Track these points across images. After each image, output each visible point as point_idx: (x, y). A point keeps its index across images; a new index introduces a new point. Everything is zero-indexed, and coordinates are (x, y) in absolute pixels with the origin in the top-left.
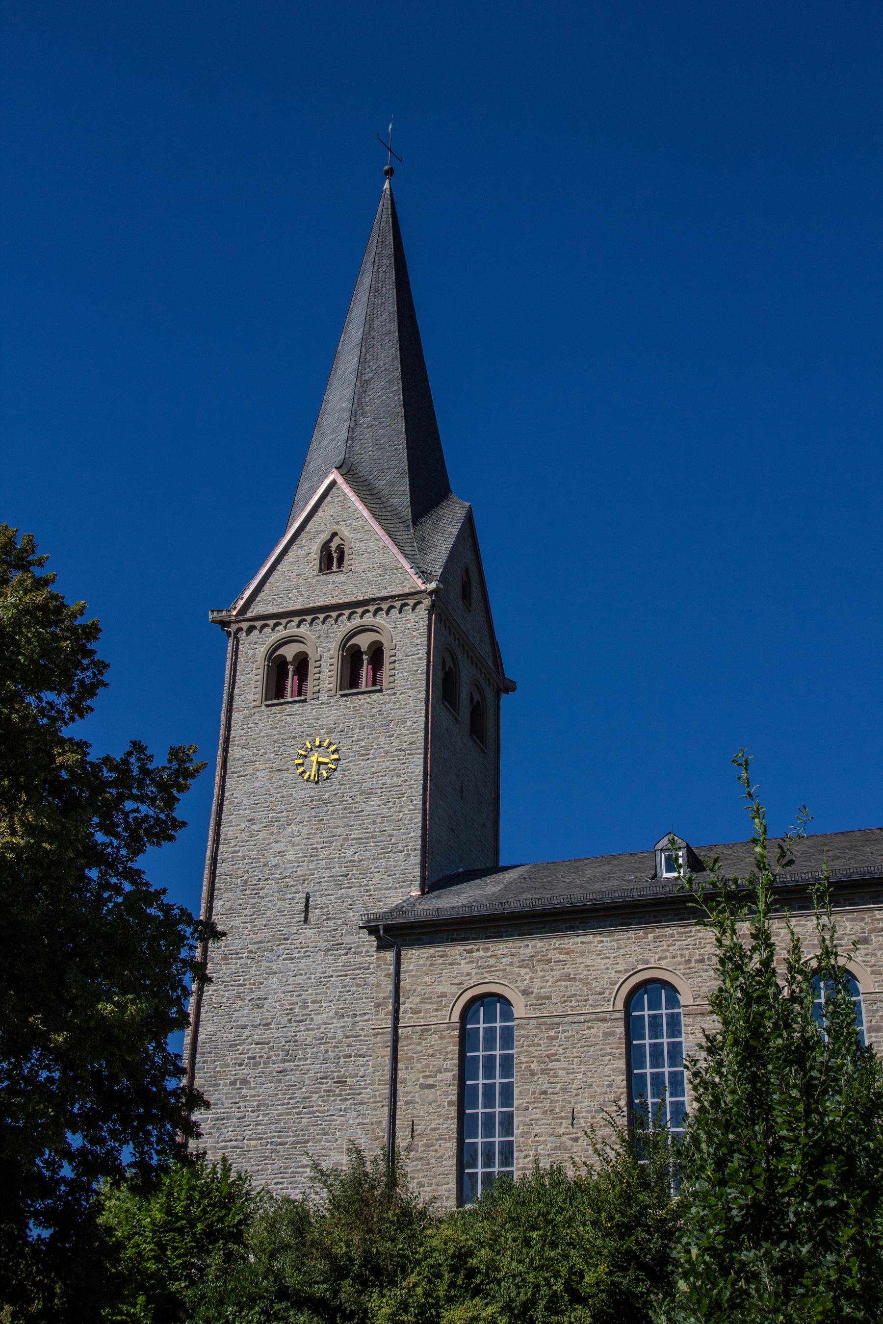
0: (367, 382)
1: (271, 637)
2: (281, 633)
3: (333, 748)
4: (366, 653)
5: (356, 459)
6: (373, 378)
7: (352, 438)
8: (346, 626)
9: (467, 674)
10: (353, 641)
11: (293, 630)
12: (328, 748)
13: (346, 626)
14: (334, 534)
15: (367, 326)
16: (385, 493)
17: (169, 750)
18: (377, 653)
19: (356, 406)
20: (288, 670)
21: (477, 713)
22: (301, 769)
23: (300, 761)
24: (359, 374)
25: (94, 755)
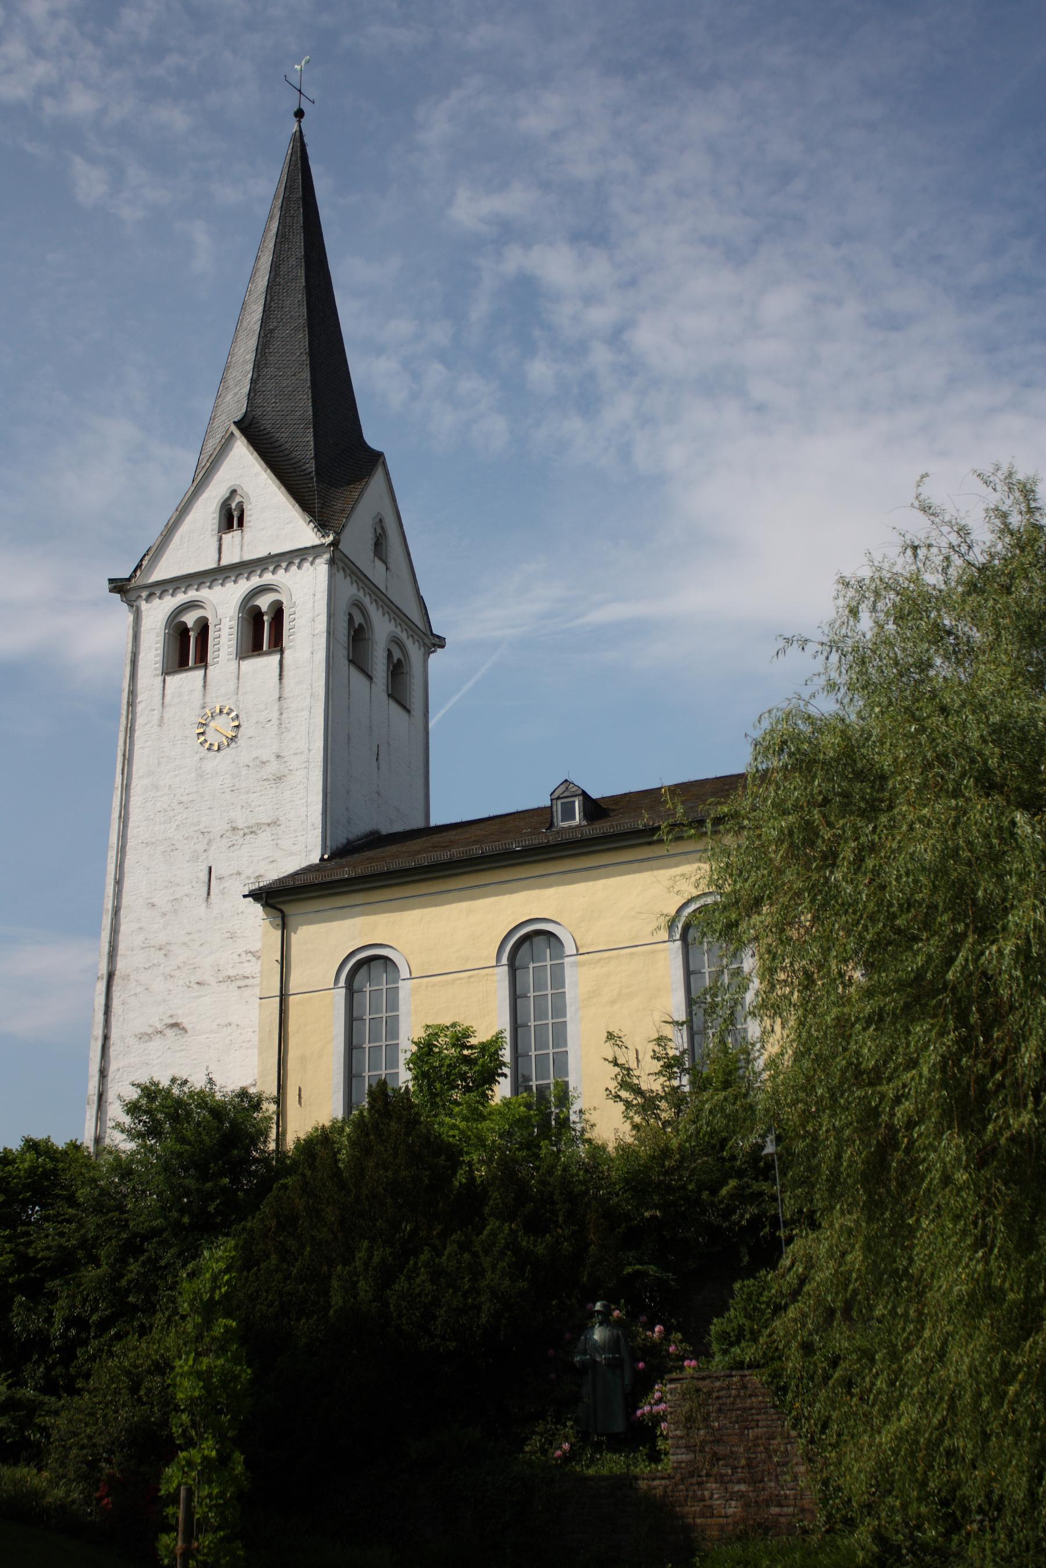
0: (271, 331)
1: (167, 604)
2: (181, 598)
3: (233, 714)
4: (192, 629)
5: (258, 412)
6: (277, 327)
7: (255, 390)
8: (243, 586)
9: (382, 628)
10: (177, 621)
11: (192, 594)
12: (228, 714)
13: (243, 586)
14: (234, 492)
15: (273, 273)
16: (287, 446)
17: (606, 1035)
18: (278, 611)
19: (259, 356)
20: (189, 637)
21: (397, 670)
22: (202, 738)
23: (201, 730)
24: (264, 321)
25: (161, 1086)
